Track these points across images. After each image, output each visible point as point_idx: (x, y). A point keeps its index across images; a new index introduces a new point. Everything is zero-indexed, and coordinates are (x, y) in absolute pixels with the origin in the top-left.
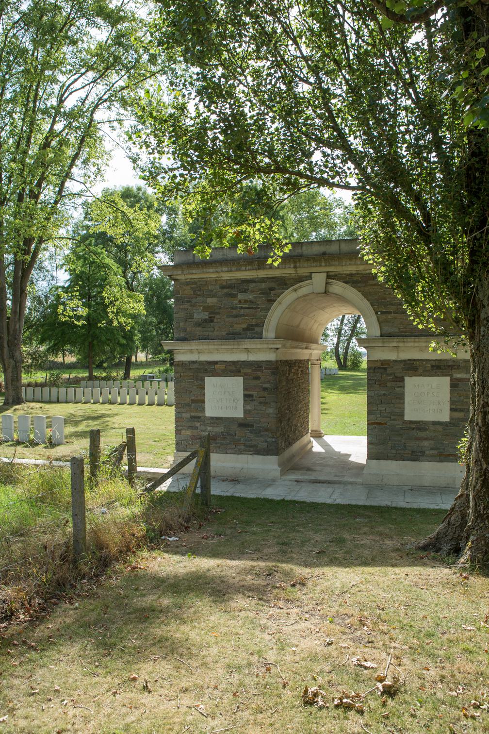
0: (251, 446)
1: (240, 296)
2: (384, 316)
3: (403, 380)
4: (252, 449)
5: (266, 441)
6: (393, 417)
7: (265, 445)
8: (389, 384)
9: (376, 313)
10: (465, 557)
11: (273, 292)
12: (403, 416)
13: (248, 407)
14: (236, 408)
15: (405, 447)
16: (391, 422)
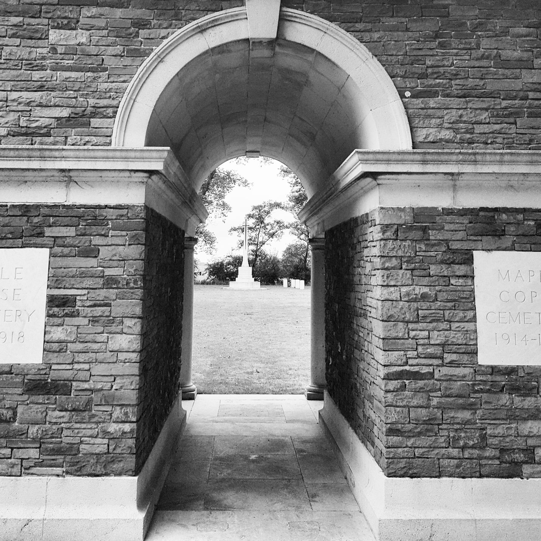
0: (58, 451)
1: (54, 36)
2: (418, 102)
3: (469, 261)
4: (60, 459)
5: (106, 433)
6: (448, 358)
7: (100, 445)
8: (434, 269)
9: (402, 96)
10: (330, 209)
11: (143, 33)
12: (475, 353)
13: (58, 334)
14: (21, 336)
15: (483, 437)
16: (445, 370)
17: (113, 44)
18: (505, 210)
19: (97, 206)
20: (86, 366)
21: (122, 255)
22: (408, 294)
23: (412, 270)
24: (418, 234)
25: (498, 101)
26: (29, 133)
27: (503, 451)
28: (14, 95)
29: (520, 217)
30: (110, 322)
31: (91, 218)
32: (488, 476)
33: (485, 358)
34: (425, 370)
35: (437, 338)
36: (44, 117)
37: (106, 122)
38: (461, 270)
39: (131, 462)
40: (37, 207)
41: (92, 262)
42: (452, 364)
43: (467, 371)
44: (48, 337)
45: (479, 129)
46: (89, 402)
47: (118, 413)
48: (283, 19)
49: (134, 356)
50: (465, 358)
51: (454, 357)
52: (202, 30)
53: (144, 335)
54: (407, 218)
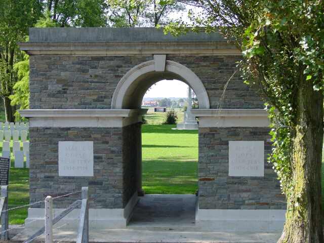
1: (91, 71)
3: (227, 144)
5: (113, 196)
8: (216, 147)
12: (227, 172)
13: (98, 168)
17: (110, 73)
18: (240, 128)
19: (188, 45)
20: (106, 177)
21: (116, 144)
22: (208, 155)
23: (209, 147)
24: (211, 136)
25: (239, 91)
26: (85, 104)
27: (235, 201)
28: (79, 92)
29: (244, 130)
30: (114, 164)
31: (106, 131)
32: (230, 209)
33: (230, 174)
34: (212, 178)
35: (216, 168)
36: (89, 99)
37: (109, 100)
38: (224, 147)
39: (122, 205)
40: (89, 128)
41: (107, 145)
42: (220, 176)
43: (226, 178)
44: (95, 168)
45: (232, 101)
46: (108, 187)
47: (117, 190)
48: (166, 64)
49: (121, 174)
50: (225, 174)
51: (221, 174)
52: (139, 68)
53: (124, 168)
54: (208, 131)
